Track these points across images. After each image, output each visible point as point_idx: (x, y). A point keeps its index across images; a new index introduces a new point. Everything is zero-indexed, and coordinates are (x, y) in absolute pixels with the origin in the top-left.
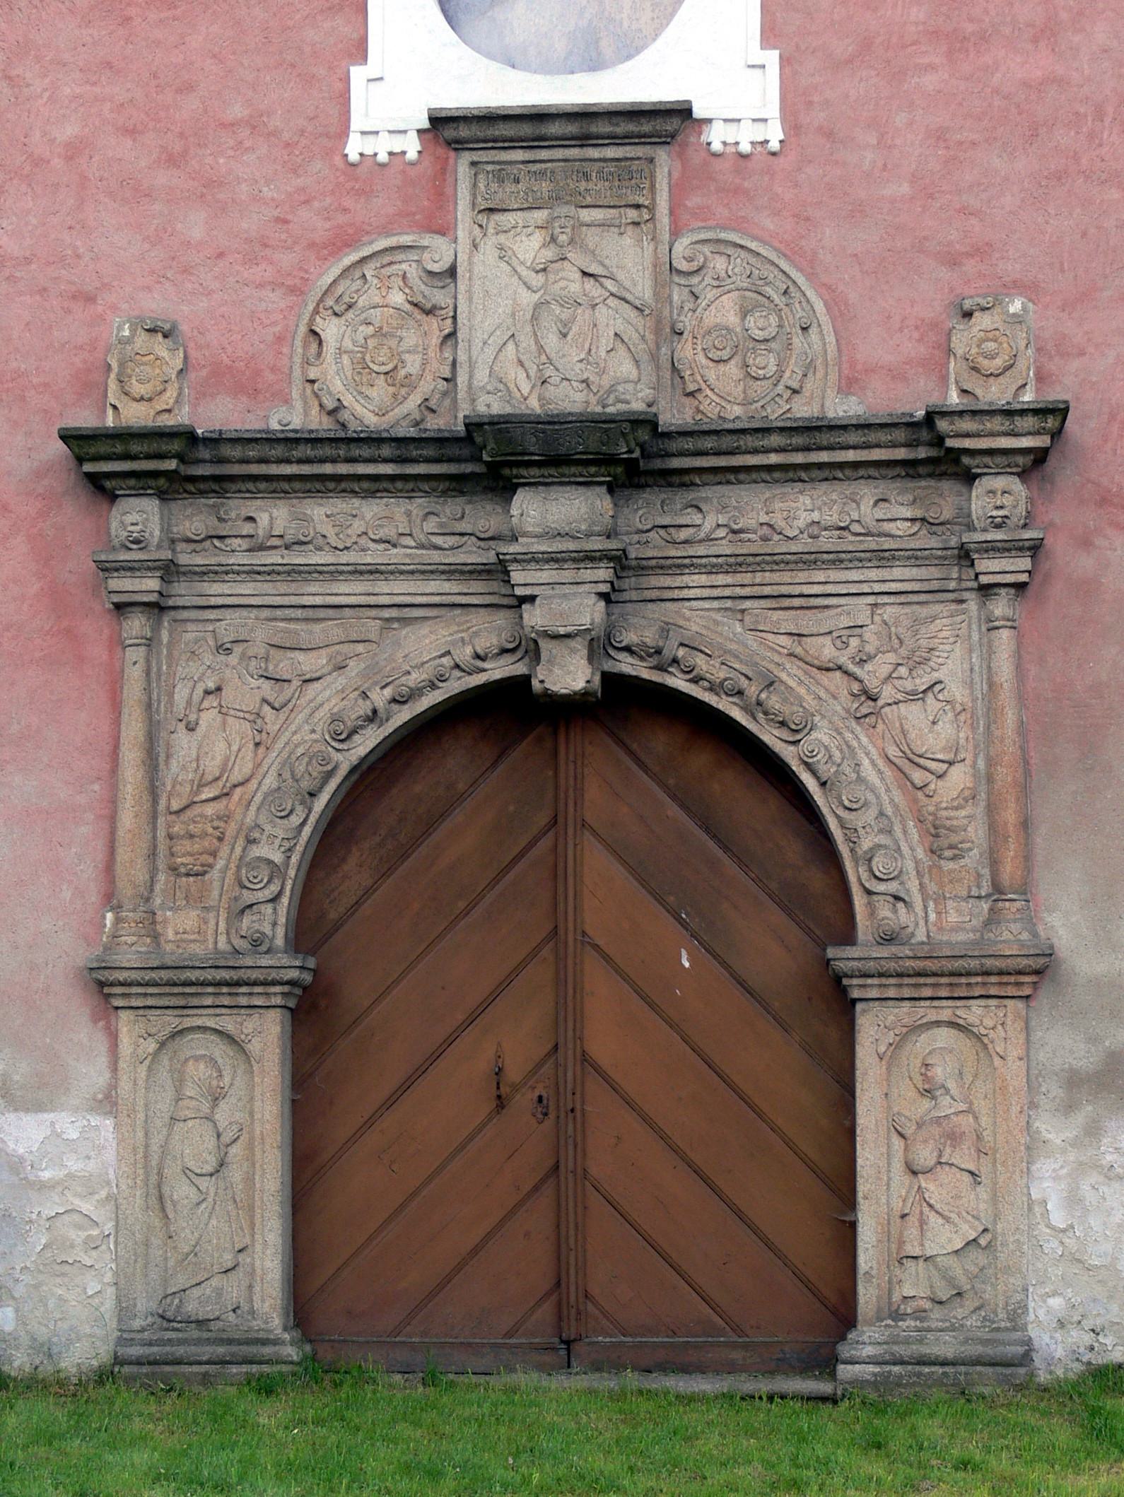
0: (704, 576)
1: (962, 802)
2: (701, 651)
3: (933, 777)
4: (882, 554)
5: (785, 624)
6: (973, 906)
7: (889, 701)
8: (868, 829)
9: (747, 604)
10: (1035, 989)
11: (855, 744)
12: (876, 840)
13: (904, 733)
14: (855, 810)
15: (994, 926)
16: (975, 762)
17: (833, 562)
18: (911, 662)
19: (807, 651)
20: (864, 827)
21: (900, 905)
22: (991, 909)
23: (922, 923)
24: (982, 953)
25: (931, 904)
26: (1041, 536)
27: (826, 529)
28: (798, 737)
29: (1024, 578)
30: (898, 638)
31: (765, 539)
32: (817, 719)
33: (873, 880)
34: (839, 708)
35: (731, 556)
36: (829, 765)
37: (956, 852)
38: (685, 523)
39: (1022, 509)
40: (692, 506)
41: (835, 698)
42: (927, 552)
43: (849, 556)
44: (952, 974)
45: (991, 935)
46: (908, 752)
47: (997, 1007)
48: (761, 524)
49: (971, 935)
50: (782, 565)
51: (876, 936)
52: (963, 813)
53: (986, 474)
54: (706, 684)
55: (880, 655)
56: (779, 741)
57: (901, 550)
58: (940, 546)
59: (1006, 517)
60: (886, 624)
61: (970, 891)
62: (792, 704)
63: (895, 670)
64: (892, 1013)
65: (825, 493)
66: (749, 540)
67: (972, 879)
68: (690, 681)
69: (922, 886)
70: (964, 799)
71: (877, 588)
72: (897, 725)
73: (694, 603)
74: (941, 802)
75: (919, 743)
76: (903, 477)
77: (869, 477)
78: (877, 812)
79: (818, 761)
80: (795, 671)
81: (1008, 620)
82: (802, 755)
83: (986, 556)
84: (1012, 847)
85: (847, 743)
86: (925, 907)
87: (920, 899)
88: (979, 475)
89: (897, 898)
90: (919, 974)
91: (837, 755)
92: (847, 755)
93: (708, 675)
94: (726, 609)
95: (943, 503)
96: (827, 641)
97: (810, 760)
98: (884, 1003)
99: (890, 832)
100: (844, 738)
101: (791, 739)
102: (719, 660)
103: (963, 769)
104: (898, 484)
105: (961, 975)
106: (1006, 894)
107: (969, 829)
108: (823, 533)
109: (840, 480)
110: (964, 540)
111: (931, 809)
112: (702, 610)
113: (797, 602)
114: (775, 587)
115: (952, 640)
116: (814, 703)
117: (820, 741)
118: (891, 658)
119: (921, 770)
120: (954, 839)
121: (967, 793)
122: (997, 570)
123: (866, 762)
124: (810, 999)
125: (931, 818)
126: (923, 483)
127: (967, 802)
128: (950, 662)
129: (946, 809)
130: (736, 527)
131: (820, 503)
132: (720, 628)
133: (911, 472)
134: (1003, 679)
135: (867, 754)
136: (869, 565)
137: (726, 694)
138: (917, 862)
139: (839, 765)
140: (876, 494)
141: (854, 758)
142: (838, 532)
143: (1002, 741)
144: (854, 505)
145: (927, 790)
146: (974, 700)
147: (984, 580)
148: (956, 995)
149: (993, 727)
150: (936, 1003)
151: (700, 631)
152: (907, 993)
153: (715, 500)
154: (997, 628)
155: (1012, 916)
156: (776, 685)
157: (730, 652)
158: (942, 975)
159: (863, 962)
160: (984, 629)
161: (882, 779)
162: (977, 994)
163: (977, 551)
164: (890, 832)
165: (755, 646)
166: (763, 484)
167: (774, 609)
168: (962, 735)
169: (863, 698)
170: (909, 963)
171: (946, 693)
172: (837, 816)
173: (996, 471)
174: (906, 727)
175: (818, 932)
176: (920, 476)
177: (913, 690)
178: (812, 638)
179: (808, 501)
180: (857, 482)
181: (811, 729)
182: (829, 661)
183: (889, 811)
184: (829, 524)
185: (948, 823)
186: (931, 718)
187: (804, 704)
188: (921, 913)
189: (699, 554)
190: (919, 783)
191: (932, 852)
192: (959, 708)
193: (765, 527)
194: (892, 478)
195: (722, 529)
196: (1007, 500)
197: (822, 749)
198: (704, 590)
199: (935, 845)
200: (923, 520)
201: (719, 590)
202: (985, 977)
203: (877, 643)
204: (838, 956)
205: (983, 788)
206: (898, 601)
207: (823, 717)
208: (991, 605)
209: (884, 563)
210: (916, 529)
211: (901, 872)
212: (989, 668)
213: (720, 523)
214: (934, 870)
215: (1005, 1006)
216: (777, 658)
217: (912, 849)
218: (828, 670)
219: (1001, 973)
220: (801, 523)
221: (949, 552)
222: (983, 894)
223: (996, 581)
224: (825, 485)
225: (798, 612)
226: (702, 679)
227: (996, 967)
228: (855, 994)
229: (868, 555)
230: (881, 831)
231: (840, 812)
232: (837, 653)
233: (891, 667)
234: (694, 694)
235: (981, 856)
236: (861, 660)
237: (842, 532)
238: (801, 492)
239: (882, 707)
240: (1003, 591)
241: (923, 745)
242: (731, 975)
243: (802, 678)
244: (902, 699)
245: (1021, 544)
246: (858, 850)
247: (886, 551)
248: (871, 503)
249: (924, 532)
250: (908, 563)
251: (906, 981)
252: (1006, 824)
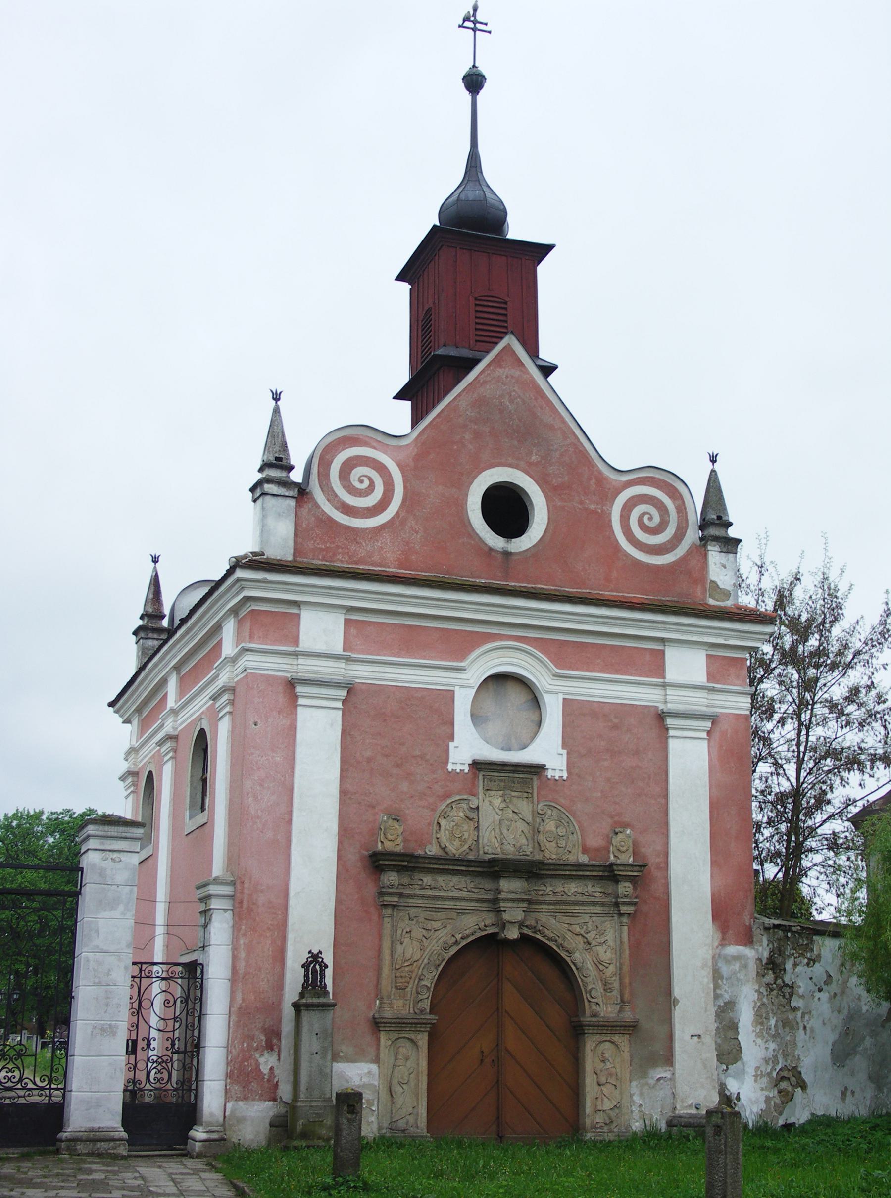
9: (557, 914)
44: (612, 1026)
69: (603, 1001)
71: (592, 912)
89: (597, 1003)
96: (577, 926)
113: (571, 915)
118: (595, 932)
120: (610, 986)
147: (622, 912)
200: (604, 892)
220: (572, 891)
231: (582, 977)
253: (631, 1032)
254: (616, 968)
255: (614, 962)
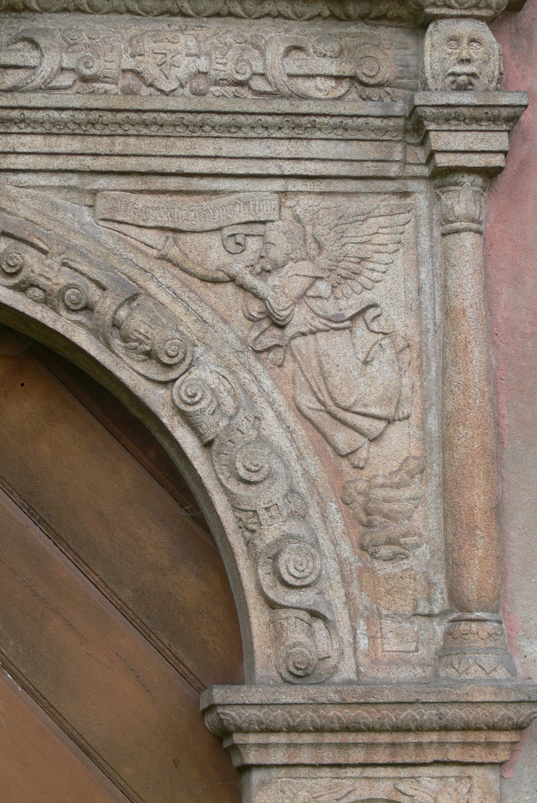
0: (39, 138)
1: (406, 477)
2: (33, 245)
3: (365, 440)
4: (297, 120)
5: (155, 213)
6: (420, 629)
7: (304, 329)
8: (273, 513)
9: (102, 182)
10: (513, 752)
11: (254, 388)
12: (285, 528)
13: (324, 375)
14: (255, 483)
15: (455, 659)
16: (424, 421)
17: (228, 127)
18: (333, 276)
19: (186, 254)
20: (267, 509)
21: (318, 625)
22: (448, 634)
23: (349, 651)
24: (440, 698)
25: (362, 625)
26: (524, 102)
27: (216, 83)
28: (172, 375)
29: (497, 161)
30: (316, 241)
31: (128, 92)
32: (199, 350)
33: (279, 587)
34: (231, 337)
35: (80, 109)
36: (217, 417)
37: (397, 549)
38: (13, 63)
39: (494, 67)
40: (24, 39)
41: (226, 322)
42: (361, 121)
43: (251, 120)
44: (396, 729)
45: (451, 672)
46: (329, 403)
47: (459, 778)
48: (124, 71)
49: (419, 671)
50: (154, 128)
51: (283, 671)
52: (407, 493)
53: (444, 17)
54: (38, 293)
55: (291, 263)
56: (143, 381)
57: (325, 115)
58: (379, 112)
59: (473, 75)
60: (299, 221)
61: (416, 607)
62: (164, 326)
63: (311, 285)
64: (305, 786)
65: (216, 34)
66: (106, 92)
67: (420, 588)
68: (15, 288)
69: (349, 597)
70: (408, 472)
71: (289, 168)
72: (314, 363)
73: (24, 178)
74: (375, 476)
75: (345, 390)
76: (325, 19)
77: (280, 15)
78: (286, 487)
79: (202, 411)
80: (168, 281)
81: (473, 221)
82: (177, 401)
83: (445, 127)
84: (481, 542)
85: (242, 386)
86: (354, 629)
87: (346, 617)
88: (435, 18)
89: (315, 614)
90: (347, 729)
91: (229, 404)
92: (244, 403)
93: (42, 281)
94: (70, 188)
95: (381, 57)
96: (215, 240)
97: (190, 409)
98: (293, 771)
99: (304, 517)
100: (238, 379)
101: (161, 378)
102: (58, 259)
103: (407, 430)
104: (318, 28)
105: (408, 730)
106: (471, 612)
107: (415, 516)
108: (213, 89)
109: (238, 16)
110: (417, 102)
111: (362, 486)
112: (34, 187)
113: (173, 183)
114: (142, 160)
115: (391, 247)
116: (195, 328)
117: (204, 382)
118: (306, 268)
119: (348, 430)
120: (395, 530)
121: (412, 464)
122: (462, 148)
123: (269, 415)
124: (176, 763)
125: (360, 499)
126: (353, 29)
127: (412, 477)
128: (388, 278)
129: (382, 486)
130: (87, 72)
131: (208, 47)
132: (60, 215)
133: (338, 11)
134: (467, 303)
135: (271, 404)
136: (278, 134)
137: (68, 309)
138: (341, 562)
139: (231, 418)
140: (287, 39)
141: (252, 408)
142: (233, 89)
143: (465, 389)
144: (256, 53)
145: (355, 459)
146: (423, 333)
147: (442, 160)
148: (399, 760)
149: (451, 371)
150: (369, 772)
151: (32, 217)
152: (328, 756)
153: (58, 34)
154: (457, 231)
155: (482, 645)
156: (141, 299)
157: (74, 248)
158: (381, 731)
159: (265, 710)
160: (437, 233)
161: (293, 441)
162: (430, 759)
163: (435, 120)
164: (303, 517)
165: (111, 243)
166: (127, 16)
167: (141, 192)
168: (406, 381)
169: (265, 324)
170: (333, 712)
171: (383, 323)
172: (227, 492)
173: (459, 12)
174: (327, 367)
175: (189, 663)
176: (349, 18)
177: (337, 315)
178: (195, 237)
179: (192, 44)
180: (262, 21)
181: (191, 365)
182: (218, 270)
183: (302, 487)
184: (222, 75)
185: (386, 507)
186: (362, 356)
187: (181, 328)
188: (347, 638)
189: (33, 104)
190: (344, 448)
191: (363, 548)
192: (401, 344)
193: (129, 76)
194: (308, 20)
195: (66, 74)
196: (475, 52)
197: (208, 393)
198: (38, 158)
199: (368, 538)
200: (353, 78)
201: (61, 159)
202: (443, 734)
203: (286, 246)
204: (230, 700)
205: (436, 457)
206: (317, 189)
207: (209, 348)
208: (448, 199)
209: (299, 132)
210: (343, 91)
211: (319, 576)
212: (445, 287)
213: (64, 65)
214: (366, 575)
215: (470, 777)
216: (142, 262)
217: (335, 544)
218: (215, 281)
219: (466, 728)
220: (181, 72)
221: (392, 123)
222: (436, 611)
223: (459, 164)
224: (215, 23)
225: (175, 198)
226: (32, 285)
227: (461, 718)
228: (252, 758)
229: (278, 119)
230: (292, 515)
231: (233, 486)
232: (229, 259)
233: (306, 282)
234: (20, 307)
235: (432, 556)
236: (263, 269)
237: (238, 88)
238: (182, 31)
239: (293, 338)
240: (467, 179)
241: (351, 394)
242: (61, 726)
243: (179, 292)
244: (321, 327)
245: (496, 112)
246: (257, 542)
247: (304, 115)
248: (282, 49)
249: (354, 95)
250: (332, 136)
251: (328, 738)
252: (471, 509)
253: (502, 755)
254: (424, 440)
255: (416, 414)
